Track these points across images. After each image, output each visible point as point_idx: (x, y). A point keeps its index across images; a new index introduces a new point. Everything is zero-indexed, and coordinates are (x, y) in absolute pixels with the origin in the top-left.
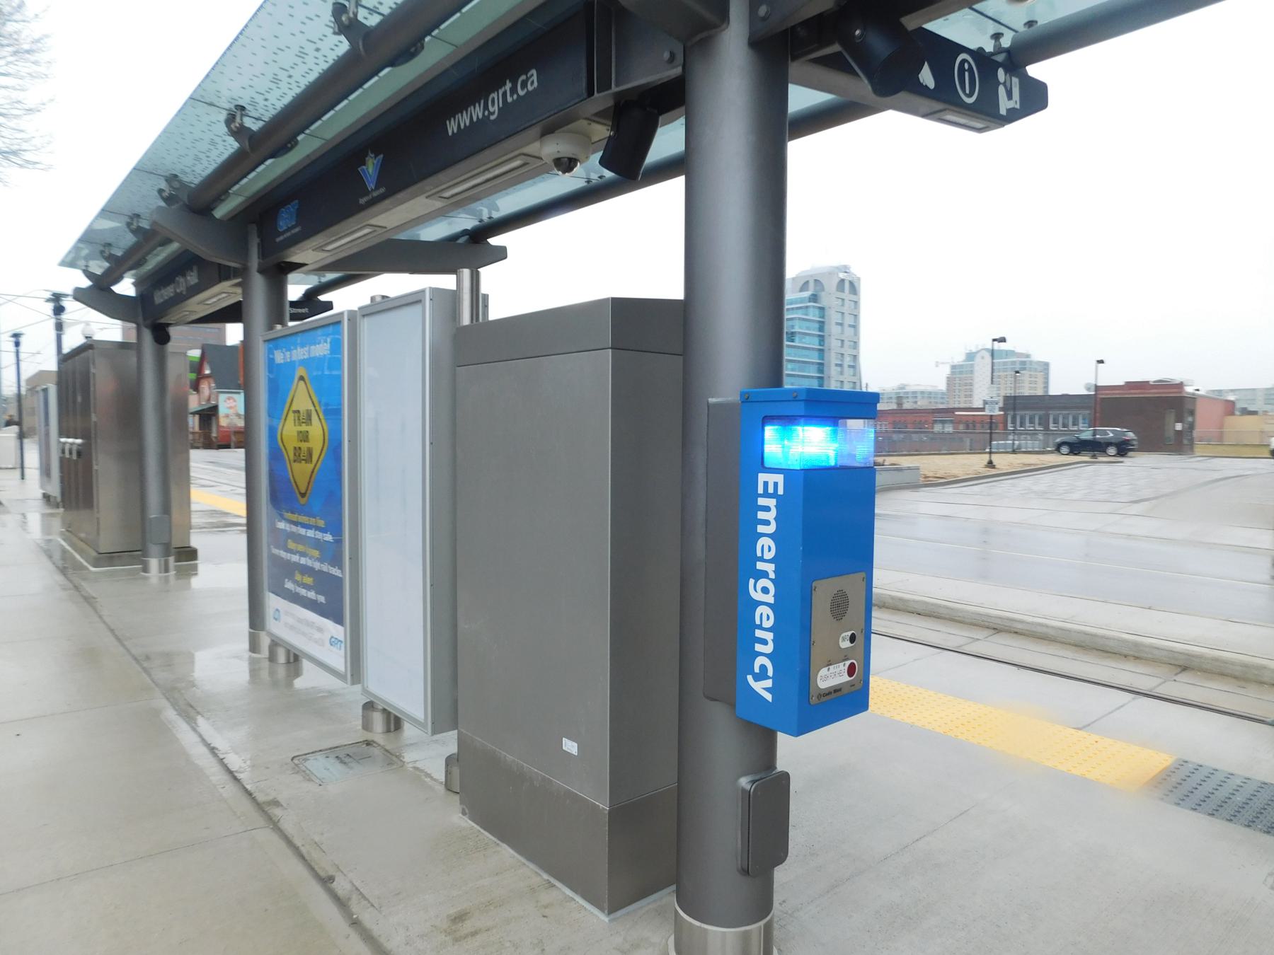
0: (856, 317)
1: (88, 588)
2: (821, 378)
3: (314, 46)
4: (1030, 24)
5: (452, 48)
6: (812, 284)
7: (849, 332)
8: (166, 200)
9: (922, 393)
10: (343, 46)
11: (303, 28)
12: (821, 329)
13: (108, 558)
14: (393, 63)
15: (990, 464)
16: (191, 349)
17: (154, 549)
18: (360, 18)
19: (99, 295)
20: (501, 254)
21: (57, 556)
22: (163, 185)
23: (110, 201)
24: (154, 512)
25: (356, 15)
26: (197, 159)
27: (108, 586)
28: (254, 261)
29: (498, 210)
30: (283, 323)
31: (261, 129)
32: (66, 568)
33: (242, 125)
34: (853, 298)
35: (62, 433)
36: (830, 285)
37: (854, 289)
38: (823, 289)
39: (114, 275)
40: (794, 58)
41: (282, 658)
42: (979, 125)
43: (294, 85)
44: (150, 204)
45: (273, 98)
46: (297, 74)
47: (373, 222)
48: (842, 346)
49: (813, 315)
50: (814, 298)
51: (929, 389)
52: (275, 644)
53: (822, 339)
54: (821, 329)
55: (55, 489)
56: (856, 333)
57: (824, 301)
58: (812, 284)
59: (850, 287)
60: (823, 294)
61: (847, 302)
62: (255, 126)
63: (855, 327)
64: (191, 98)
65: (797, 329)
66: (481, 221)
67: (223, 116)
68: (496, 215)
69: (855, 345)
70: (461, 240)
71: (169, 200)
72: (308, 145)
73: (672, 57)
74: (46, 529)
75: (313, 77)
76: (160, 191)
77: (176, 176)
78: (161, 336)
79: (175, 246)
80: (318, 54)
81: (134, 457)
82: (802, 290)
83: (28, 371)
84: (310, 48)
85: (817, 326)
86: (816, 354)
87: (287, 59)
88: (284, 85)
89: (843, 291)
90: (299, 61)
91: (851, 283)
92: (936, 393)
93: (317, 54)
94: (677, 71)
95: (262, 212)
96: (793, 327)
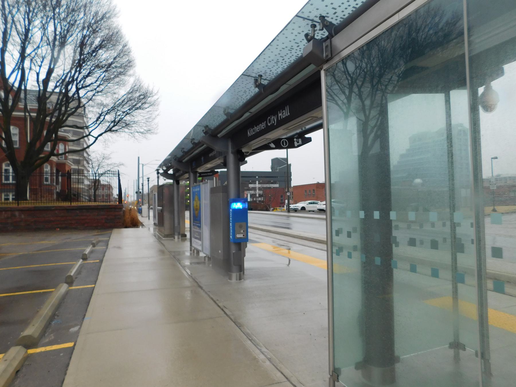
1: (163, 242)
3: (282, 58)
8: (205, 133)
10: (257, 90)
13: (167, 236)
16: (373, 216)
17: (176, 233)
18: (262, 82)
19: (165, 174)
20: (309, 140)
21: (157, 236)
22: (203, 129)
24: (176, 225)
26: (214, 121)
27: (167, 242)
28: (190, 170)
30: (196, 183)
31: (268, 84)
32: (159, 239)
35: (159, 206)
39: (168, 169)
41: (195, 252)
52: (195, 248)
55: (157, 222)
62: (265, 82)
64: (297, 16)
71: (206, 133)
72: (284, 88)
74: (154, 229)
76: (307, 35)
78: (178, 183)
79: (205, 146)
80: (298, 48)
81: (172, 212)
83: (151, 185)
84: (247, 90)
88: (247, 93)
95: (191, 161)
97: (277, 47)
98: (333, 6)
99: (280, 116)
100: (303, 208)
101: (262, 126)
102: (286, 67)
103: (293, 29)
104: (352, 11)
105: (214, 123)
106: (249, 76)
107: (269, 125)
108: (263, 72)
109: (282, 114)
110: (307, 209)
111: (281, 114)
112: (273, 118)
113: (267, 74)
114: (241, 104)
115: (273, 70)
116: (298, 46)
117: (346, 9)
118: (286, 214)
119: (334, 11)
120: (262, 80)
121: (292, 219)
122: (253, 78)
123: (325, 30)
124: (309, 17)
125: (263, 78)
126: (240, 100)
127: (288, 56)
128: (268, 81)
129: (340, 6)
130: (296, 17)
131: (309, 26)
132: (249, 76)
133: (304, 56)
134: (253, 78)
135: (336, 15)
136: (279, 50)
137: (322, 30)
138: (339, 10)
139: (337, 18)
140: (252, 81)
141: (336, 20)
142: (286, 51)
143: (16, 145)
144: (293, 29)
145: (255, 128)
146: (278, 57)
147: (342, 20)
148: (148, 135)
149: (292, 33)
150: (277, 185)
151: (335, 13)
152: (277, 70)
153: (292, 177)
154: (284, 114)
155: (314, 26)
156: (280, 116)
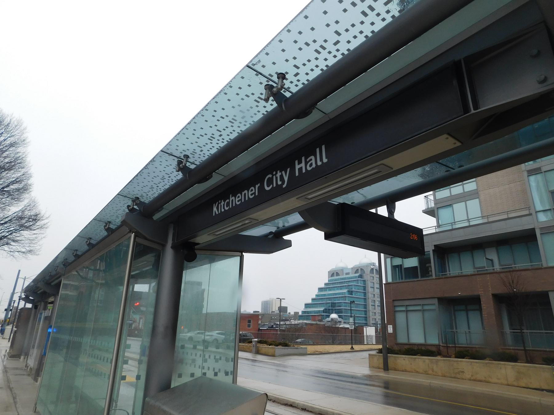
2: (366, 311)
3: (200, 149)
4: (284, 226)
5: (222, 177)
6: (359, 270)
10: (180, 175)
14: (200, 181)
15: (352, 348)
18: (187, 165)
19: (27, 300)
20: (288, 244)
22: (130, 203)
23: (176, 138)
25: (185, 165)
29: (288, 223)
31: (195, 168)
33: (133, 208)
36: (368, 271)
38: (364, 272)
43: (170, 181)
45: (160, 186)
46: (160, 186)
47: (251, 216)
49: (360, 284)
50: (361, 276)
53: (365, 294)
54: (365, 289)
58: (359, 270)
60: (364, 275)
61: (375, 278)
64: (162, 151)
65: (353, 290)
66: (278, 228)
68: (287, 225)
70: (270, 236)
72: (216, 179)
75: (167, 187)
76: (128, 206)
77: (138, 198)
79: (42, 290)
80: (220, 138)
82: (355, 273)
84: (166, 176)
86: (363, 300)
87: (157, 180)
88: (166, 181)
89: (373, 273)
90: (151, 190)
97: (239, 91)
98: (296, 62)
99: (300, 169)
105: (97, 237)
106: (125, 197)
107: (267, 188)
108: (191, 151)
109: (306, 163)
111: (303, 165)
112: (279, 174)
113: (196, 156)
116: (202, 151)
119: (296, 71)
122: (176, 159)
125: (189, 160)
127: (228, 131)
131: (263, 86)
132: (125, 197)
134: (176, 159)
136: (216, 118)
140: (175, 163)
142: (205, 140)
146: (163, 173)
148: (29, 255)
152: (211, 149)
155: (133, 201)
156: (300, 169)
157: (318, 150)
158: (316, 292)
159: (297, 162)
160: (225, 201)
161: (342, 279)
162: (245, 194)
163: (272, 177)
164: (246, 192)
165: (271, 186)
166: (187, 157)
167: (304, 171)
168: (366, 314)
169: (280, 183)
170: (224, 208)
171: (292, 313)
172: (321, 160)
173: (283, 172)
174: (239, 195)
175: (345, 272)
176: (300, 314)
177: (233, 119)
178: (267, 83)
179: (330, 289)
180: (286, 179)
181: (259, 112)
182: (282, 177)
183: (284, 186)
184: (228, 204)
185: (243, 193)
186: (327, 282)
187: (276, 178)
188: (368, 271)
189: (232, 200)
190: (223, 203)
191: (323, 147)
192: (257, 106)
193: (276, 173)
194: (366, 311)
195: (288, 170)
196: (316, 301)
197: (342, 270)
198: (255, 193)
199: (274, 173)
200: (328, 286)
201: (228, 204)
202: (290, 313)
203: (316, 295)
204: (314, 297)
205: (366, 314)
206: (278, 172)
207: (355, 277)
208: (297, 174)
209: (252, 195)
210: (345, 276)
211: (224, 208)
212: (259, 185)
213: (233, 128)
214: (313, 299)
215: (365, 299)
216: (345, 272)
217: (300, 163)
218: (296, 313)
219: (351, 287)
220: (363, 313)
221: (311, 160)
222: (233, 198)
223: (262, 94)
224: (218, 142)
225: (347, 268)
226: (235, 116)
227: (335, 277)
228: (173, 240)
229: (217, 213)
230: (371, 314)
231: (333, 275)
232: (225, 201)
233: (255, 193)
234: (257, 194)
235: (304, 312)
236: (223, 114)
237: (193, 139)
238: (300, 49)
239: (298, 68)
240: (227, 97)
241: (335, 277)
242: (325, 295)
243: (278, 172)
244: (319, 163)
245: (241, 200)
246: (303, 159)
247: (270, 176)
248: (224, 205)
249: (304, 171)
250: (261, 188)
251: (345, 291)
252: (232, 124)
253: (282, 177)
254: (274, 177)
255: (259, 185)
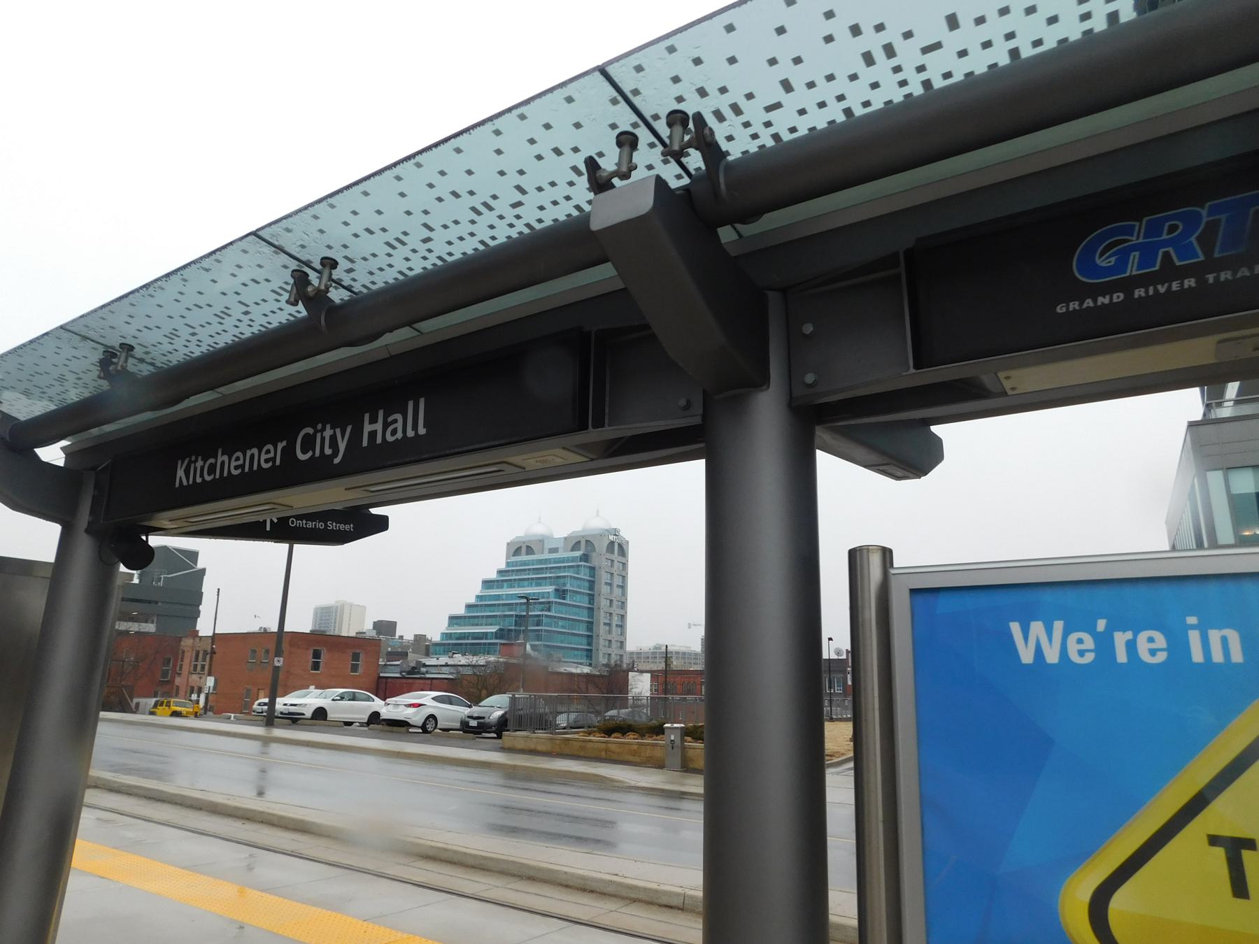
0: (624, 578)
2: (590, 637)
6: (583, 544)
7: (617, 591)
9: (677, 653)
10: (301, 311)
11: (390, 260)
12: (591, 587)
34: (621, 559)
36: (601, 547)
37: (623, 551)
38: (594, 549)
40: (820, 422)
42: (899, 474)
44: (78, 381)
48: (611, 605)
49: (584, 574)
50: (585, 558)
51: (683, 649)
53: (591, 598)
54: (591, 587)
56: (624, 594)
57: (595, 562)
58: (583, 544)
59: (618, 548)
63: (623, 587)
65: (568, 587)
67: (97, 355)
69: (623, 605)
72: (398, 339)
73: (688, 407)
80: (245, 318)
82: (573, 549)
85: (587, 584)
86: (586, 612)
87: (196, 318)
89: (613, 552)
91: (620, 546)
92: (690, 654)
93: (190, 338)
94: (697, 420)
96: (564, 584)
97: (436, 179)
99: (373, 434)
100: (320, 713)
101: (265, 457)
102: (248, 334)
103: (355, 213)
104: (476, 249)
107: (302, 457)
109: (386, 425)
110: (331, 716)
111: (378, 427)
112: (328, 433)
114: (176, 359)
115: (203, 334)
117: (555, 203)
118: (259, 731)
119: (518, 197)
120: (131, 360)
121: (275, 749)
123: (301, 307)
124: (636, 92)
125: (336, 274)
126: (179, 343)
127: (551, 194)
128: (151, 368)
129: (445, 227)
130: (597, 74)
133: (595, 225)
135: (429, 245)
137: (295, 304)
138: (440, 236)
139: (427, 255)
141: (425, 258)
143: (594, 565)
144: (355, 213)
145: (222, 458)
147: (439, 263)
149: (431, 186)
150: (150, 628)
151: (518, 204)
153: (201, 608)
154: (409, 424)
156: (373, 434)
157: (411, 404)
158: (477, 589)
159: (367, 417)
160: (205, 460)
161: (540, 562)
162: (252, 455)
163: (314, 435)
164: (255, 451)
165: (310, 454)
166: (329, 263)
167: (379, 440)
168: (590, 644)
169: (328, 451)
170: (202, 475)
171: (409, 637)
172: (415, 427)
173: (338, 431)
174: (239, 454)
175: (547, 546)
176: (437, 638)
177: (398, 240)
178: (630, 129)
179: (511, 583)
180: (342, 446)
181: (390, 266)
182: (333, 439)
183: (337, 460)
184: (212, 470)
185: (249, 453)
186: (503, 566)
187: (323, 439)
188: (601, 547)
189: (223, 463)
190: (200, 463)
191: (422, 401)
192: (389, 255)
193: (324, 429)
194: (590, 637)
195: (349, 429)
196: (476, 612)
197: (541, 541)
198: (273, 459)
199: (319, 426)
200: (505, 578)
201: (212, 470)
202: (401, 637)
203: (477, 597)
204: (472, 600)
205: (590, 644)
206: (328, 426)
207: (574, 559)
208: (365, 443)
209: (267, 461)
210: (546, 556)
211: (202, 475)
212: (284, 443)
213: (472, 228)
214: (469, 607)
215: (591, 610)
216: (547, 546)
217: (373, 420)
218: (419, 639)
219: (562, 581)
220: (585, 641)
221: (395, 421)
222: (226, 458)
223: (286, 283)
224: (496, 222)
225: (551, 538)
226: (405, 234)
227: (524, 558)
228: (93, 512)
229: (185, 483)
230: (601, 642)
231: (517, 552)
232: (205, 460)
233: (273, 459)
234: (278, 462)
235: (446, 636)
236: (375, 223)
237: (420, 198)
238: (539, 158)
239: (431, 229)
240: (498, 142)
241: (524, 558)
242: (498, 597)
243: (328, 426)
244: (410, 433)
245: (243, 466)
246: (381, 413)
247: (310, 430)
248: (202, 468)
249: (379, 440)
250: (289, 452)
251: (550, 589)
252: (474, 216)
253: (333, 439)
254: (319, 436)
255: (284, 443)
